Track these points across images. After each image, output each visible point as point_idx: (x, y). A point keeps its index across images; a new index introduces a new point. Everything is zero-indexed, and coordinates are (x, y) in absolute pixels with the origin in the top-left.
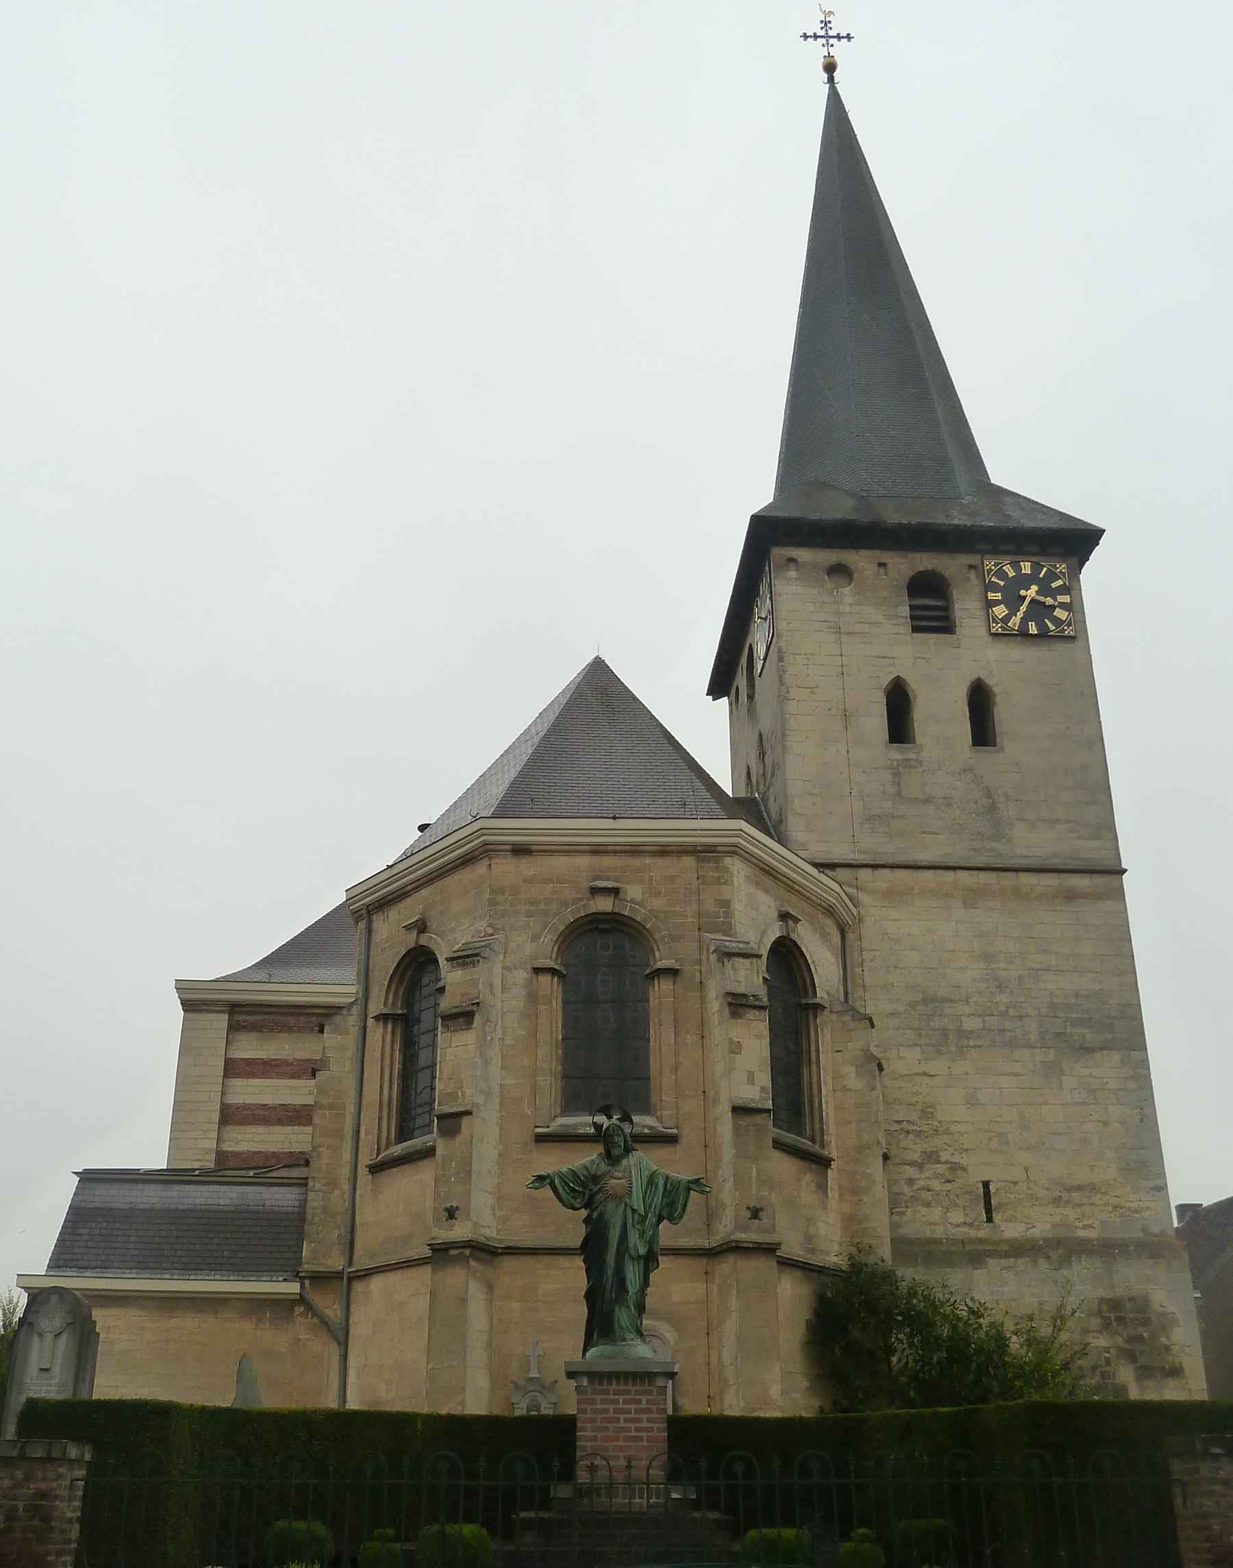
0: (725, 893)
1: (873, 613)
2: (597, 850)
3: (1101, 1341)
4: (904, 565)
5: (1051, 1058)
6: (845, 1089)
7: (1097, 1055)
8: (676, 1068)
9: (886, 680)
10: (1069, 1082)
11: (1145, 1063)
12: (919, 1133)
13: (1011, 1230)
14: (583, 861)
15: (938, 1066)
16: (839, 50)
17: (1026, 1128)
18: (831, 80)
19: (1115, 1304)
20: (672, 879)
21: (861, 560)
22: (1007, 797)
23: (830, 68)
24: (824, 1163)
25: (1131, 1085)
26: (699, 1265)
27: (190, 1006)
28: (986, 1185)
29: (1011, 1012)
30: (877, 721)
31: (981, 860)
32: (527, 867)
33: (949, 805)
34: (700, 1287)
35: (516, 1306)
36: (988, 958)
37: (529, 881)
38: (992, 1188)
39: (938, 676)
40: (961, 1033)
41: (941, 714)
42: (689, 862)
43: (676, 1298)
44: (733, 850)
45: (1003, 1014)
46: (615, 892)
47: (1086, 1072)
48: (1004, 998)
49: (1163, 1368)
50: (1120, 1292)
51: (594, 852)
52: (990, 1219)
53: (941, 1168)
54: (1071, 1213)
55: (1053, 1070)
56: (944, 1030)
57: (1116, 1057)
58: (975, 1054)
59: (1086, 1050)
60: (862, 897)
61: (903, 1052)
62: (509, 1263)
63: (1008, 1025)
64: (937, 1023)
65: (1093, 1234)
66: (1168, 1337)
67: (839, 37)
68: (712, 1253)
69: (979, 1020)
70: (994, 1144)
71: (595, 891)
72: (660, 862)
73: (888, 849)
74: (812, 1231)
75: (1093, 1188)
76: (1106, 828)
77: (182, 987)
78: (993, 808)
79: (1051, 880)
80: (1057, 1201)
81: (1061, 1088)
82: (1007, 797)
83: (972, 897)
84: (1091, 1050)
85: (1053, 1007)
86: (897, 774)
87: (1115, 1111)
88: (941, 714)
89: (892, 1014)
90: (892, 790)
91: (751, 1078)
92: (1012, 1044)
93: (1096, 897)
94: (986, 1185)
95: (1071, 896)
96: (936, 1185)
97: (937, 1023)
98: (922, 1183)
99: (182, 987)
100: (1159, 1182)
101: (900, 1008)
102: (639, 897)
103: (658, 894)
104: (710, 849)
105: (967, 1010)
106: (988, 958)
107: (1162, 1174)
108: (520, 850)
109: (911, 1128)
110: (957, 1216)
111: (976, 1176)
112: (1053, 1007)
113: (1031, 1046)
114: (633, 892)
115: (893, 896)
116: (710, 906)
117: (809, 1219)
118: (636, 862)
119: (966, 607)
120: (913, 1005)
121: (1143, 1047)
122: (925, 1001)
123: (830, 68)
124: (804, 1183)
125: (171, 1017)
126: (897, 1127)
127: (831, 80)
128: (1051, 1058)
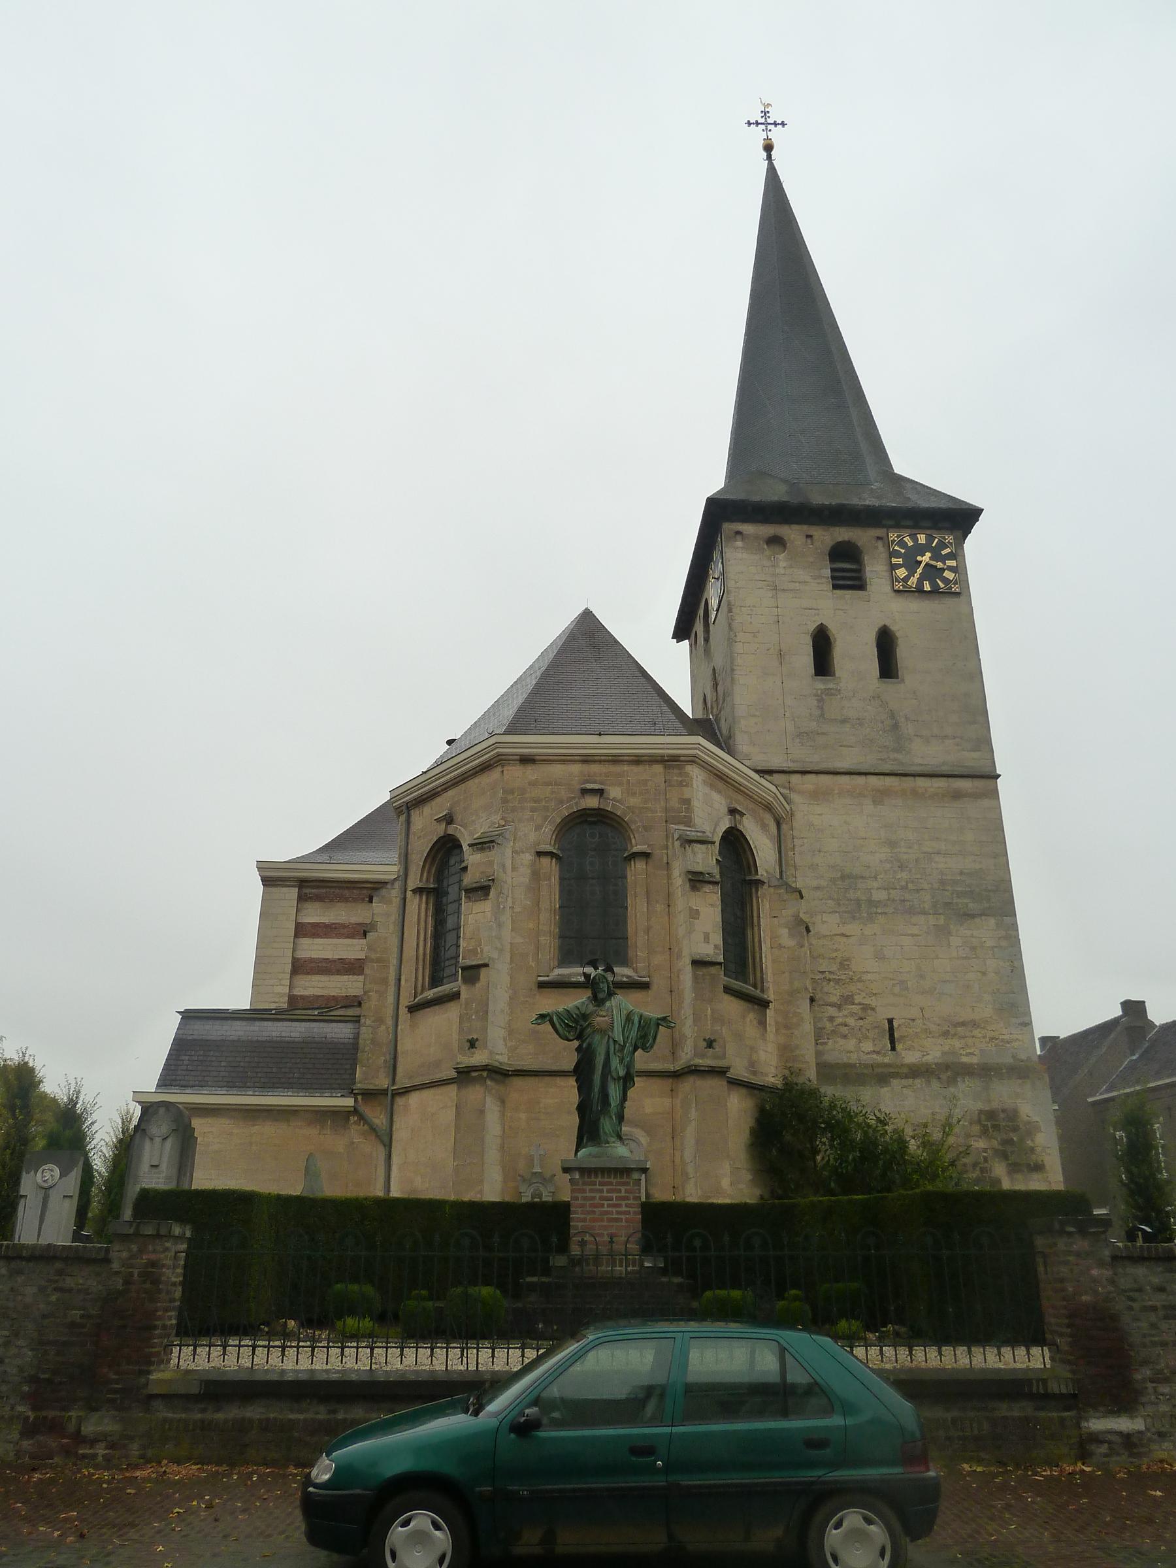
1: (802, 574)
2: (586, 760)
3: (981, 1144)
4: (827, 537)
5: (942, 922)
6: (780, 947)
7: (977, 920)
8: (648, 929)
9: (812, 627)
10: (955, 941)
11: (1014, 926)
12: (837, 981)
13: (910, 1057)
14: (576, 768)
15: (853, 928)
16: (776, 134)
17: (922, 977)
18: (769, 157)
19: (991, 1115)
20: (645, 782)
21: (793, 533)
22: (907, 719)
23: (768, 148)
24: (764, 1004)
25: (1004, 943)
26: (667, 1084)
27: (267, 881)
28: (890, 1021)
29: (910, 886)
30: (805, 659)
31: (886, 768)
32: (532, 773)
33: (861, 724)
35: (523, 1116)
36: (892, 844)
37: (533, 784)
38: (895, 1024)
39: (855, 624)
40: (871, 902)
41: (855, 653)
42: (658, 768)
44: (693, 760)
46: (600, 792)
47: (969, 933)
48: (904, 875)
50: (995, 1105)
52: (893, 1049)
54: (957, 1044)
55: (942, 932)
56: (858, 901)
57: (992, 922)
62: (518, 1082)
63: (907, 896)
64: (851, 894)
65: (974, 1060)
67: (775, 124)
70: (897, 990)
72: (635, 769)
73: (814, 759)
74: (754, 1057)
75: (974, 1024)
77: (262, 867)
78: (896, 727)
79: (941, 783)
80: (946, 1034)
81: (949, 946)
82: (907, 719)
83: (879, 797)
84: (973, 916)
85: (943, 882)
86: (821, 700)
88: (855, 653)
89: (818, 888)
90: (817, 713)
91: (707, 938)
92: (911, 911)
93: (976, 796)
94: (890, 1021)
95: (957, 795)
96: (851, 1021)
97: (851, 894)
98: (840, 1020)
99: (262, 867)
100: (1026, 1019)
101: (823, 883)
102: (619, 796)
105: (875, 885)
106: (892, 844)
107: (1028, 1013)
108: (526, 760)
109: (832, 977)
110: (868, 1046)
111: (883, 1014)
112: (943, 882)
113: (925, 913)
114: (615, 792)
115: (817, 796)
116: (674, 803)
117: (752, 1048)
120: (833, 880)
122: (843, 878)
123: (768, 148)
126: (821, 976)
127: (769, 157)
128: (942, 922)
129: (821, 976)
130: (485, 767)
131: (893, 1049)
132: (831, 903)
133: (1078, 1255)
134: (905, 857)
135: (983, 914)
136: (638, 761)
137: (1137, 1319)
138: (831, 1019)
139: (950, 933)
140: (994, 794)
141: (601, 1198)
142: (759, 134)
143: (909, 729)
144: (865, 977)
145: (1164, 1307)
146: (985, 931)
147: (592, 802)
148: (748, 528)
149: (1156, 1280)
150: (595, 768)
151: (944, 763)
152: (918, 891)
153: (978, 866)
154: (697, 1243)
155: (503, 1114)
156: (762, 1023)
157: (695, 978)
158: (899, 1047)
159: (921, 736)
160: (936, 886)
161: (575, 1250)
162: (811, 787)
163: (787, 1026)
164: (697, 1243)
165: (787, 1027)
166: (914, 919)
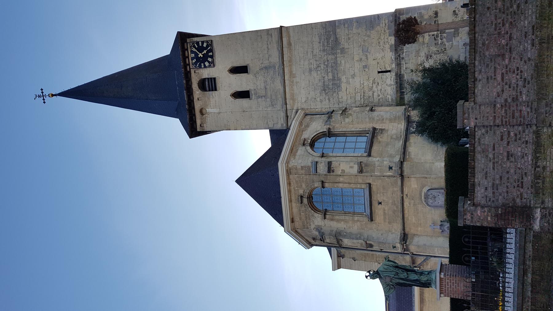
0: (299, 167)
1: (212, 101)
2: (290, 201)
4: (197, 92)
5: (339, 51)
6: (352, 121)
7: (338, 36)
8: (350, 183)
9: (232, 99)
10: (346, 46)
11: (339, 21)
12: (364, 93)
14: (294, 205)
15: (344, 86)
16: (46, 92)
17: (361, 59)
18: (55, 95)
20: (296, 182)
21: (197, 106)
22: (262, 63)
24: (374, 129)
25: (346, 26)
26: (406, 180)
27: (339, 267)
28: (379, 72)
29: (326, 63)
30: (244, 102)
31: (281, 71)
32: (297, 219)
33: (266, 81)
34: (413, 179)
35: (419, 229)
36: (310, 70)
37: (301, 219)
38: (380, 70)
39: (229, 83)
40: (334, 79)
41: (240, 82)
42: (291, 176)
43: (416, 186)
44: (288, 162)
45: (327, 66)
46: (302, 197)
47: (343, 40)
48: (322, 66)
49: (435, 17)
51: (291, 201)
52: (389, 71)
53: (374, 86)
55: (343, 51)
56: (333, 84)
57: (338, 30)
58: (340, 75)
59: (336, 40)
60: (295, 108)
61: (340, 97)
62: (407, 230)
63: (330, 65)
64: (331, 87)
66: (414, 133)
67: (42, 93)
68: (402, 176)
69: (329, 74)
70: (367, 70)
71: (302, 203)
72: (292, 184)
73: (280, 102)
74: (394, 137)
76: (268, 32)
77: (334, 269)
78: (266, 68)
81: (349, 48)
82: (262, 63)
83: (292, 75)
84: (336, 38)
85: (324, 50)
87: (355, 31)
88: (240, 82)
89: (329, 100)
90: (263, 98)
91: (351, 167)
92: (336, 63)
93: (288, 33)
94: (379, 72)
95: (290, 44)
96: (379, 88)
97: (331, 87)
98: (379, 92)
99: (334, 269)
100: (376, 17)
101: (327, 98)
102: (302, 191)
103: (301, 186)
104: (287, 171)
105: (326, 77)
106: (310, 70)
107: (374, 16)
108: (293, 221)
109: (362, 95)
112: (324, 50)
113: (336, 58)
114: (301, 192)
116: (303, 172)
117: (391, 138)
118: (293, 191)
119: (206, 73)
120: (326, 94)
121: (335, 21)
122: (325, 90)
123: (53, 95)
124: (381, 139)
125: (342, 271)
126: (362, 99)
127: (55, 95)
128: (339, 51)
129: (362, 99)
130: (296, 232)
131: (389, 71)
132: (334, 95)
133: (472, 218)
134: (315, 65)
135: (335, 34)
136: (289, 184)
137: (497, 200)
138: (379, 96)
139: (343, 48)
140: (287, 28)
141: (451, 288)
142: (47, 99)
143: (266, 63)
144: (362, 83)
145: (493, 189)
146: (342, 33)
147: (305, 201)
148: (198, 122)
149: (483, 190)
150: (293, 198)
151: (278, 49)
152: (328, 61)
153: (317, 36)
154: (467, 240)
155: (419, 236)
156: (382, 130)
157: (366, 172)
158: (389, 69)
159: (269, 58)
160: (325, 53)
161: (470, 298)
162: (291, 101)
163: (382, 120)
164: (467, 240)
165: (383, 120)
166: (339, 62)
